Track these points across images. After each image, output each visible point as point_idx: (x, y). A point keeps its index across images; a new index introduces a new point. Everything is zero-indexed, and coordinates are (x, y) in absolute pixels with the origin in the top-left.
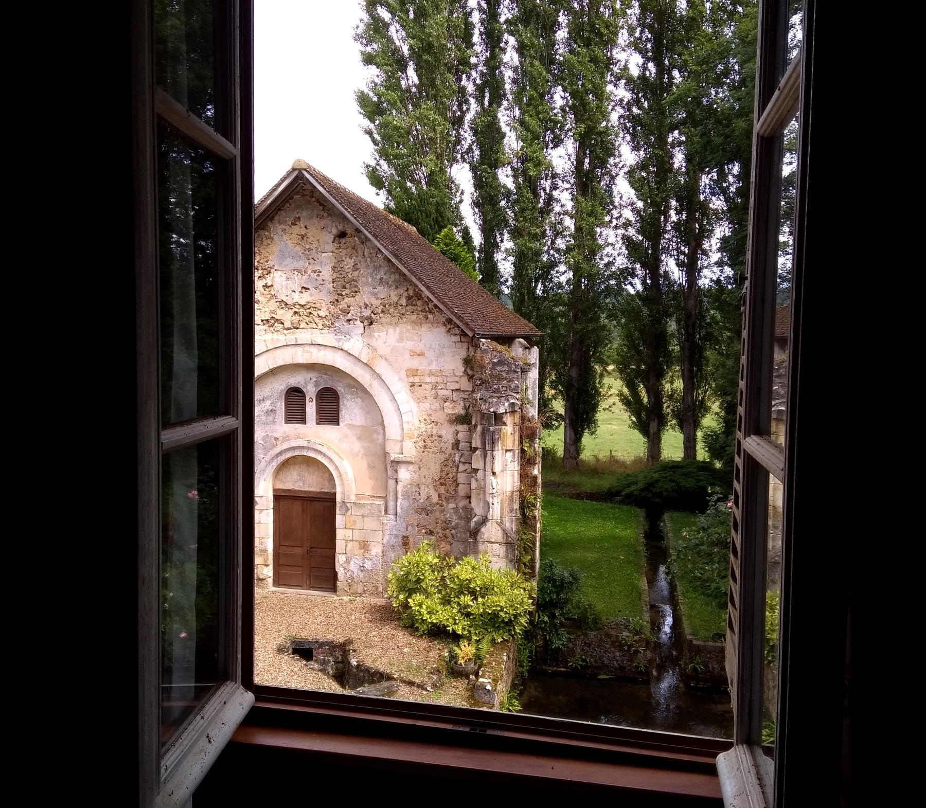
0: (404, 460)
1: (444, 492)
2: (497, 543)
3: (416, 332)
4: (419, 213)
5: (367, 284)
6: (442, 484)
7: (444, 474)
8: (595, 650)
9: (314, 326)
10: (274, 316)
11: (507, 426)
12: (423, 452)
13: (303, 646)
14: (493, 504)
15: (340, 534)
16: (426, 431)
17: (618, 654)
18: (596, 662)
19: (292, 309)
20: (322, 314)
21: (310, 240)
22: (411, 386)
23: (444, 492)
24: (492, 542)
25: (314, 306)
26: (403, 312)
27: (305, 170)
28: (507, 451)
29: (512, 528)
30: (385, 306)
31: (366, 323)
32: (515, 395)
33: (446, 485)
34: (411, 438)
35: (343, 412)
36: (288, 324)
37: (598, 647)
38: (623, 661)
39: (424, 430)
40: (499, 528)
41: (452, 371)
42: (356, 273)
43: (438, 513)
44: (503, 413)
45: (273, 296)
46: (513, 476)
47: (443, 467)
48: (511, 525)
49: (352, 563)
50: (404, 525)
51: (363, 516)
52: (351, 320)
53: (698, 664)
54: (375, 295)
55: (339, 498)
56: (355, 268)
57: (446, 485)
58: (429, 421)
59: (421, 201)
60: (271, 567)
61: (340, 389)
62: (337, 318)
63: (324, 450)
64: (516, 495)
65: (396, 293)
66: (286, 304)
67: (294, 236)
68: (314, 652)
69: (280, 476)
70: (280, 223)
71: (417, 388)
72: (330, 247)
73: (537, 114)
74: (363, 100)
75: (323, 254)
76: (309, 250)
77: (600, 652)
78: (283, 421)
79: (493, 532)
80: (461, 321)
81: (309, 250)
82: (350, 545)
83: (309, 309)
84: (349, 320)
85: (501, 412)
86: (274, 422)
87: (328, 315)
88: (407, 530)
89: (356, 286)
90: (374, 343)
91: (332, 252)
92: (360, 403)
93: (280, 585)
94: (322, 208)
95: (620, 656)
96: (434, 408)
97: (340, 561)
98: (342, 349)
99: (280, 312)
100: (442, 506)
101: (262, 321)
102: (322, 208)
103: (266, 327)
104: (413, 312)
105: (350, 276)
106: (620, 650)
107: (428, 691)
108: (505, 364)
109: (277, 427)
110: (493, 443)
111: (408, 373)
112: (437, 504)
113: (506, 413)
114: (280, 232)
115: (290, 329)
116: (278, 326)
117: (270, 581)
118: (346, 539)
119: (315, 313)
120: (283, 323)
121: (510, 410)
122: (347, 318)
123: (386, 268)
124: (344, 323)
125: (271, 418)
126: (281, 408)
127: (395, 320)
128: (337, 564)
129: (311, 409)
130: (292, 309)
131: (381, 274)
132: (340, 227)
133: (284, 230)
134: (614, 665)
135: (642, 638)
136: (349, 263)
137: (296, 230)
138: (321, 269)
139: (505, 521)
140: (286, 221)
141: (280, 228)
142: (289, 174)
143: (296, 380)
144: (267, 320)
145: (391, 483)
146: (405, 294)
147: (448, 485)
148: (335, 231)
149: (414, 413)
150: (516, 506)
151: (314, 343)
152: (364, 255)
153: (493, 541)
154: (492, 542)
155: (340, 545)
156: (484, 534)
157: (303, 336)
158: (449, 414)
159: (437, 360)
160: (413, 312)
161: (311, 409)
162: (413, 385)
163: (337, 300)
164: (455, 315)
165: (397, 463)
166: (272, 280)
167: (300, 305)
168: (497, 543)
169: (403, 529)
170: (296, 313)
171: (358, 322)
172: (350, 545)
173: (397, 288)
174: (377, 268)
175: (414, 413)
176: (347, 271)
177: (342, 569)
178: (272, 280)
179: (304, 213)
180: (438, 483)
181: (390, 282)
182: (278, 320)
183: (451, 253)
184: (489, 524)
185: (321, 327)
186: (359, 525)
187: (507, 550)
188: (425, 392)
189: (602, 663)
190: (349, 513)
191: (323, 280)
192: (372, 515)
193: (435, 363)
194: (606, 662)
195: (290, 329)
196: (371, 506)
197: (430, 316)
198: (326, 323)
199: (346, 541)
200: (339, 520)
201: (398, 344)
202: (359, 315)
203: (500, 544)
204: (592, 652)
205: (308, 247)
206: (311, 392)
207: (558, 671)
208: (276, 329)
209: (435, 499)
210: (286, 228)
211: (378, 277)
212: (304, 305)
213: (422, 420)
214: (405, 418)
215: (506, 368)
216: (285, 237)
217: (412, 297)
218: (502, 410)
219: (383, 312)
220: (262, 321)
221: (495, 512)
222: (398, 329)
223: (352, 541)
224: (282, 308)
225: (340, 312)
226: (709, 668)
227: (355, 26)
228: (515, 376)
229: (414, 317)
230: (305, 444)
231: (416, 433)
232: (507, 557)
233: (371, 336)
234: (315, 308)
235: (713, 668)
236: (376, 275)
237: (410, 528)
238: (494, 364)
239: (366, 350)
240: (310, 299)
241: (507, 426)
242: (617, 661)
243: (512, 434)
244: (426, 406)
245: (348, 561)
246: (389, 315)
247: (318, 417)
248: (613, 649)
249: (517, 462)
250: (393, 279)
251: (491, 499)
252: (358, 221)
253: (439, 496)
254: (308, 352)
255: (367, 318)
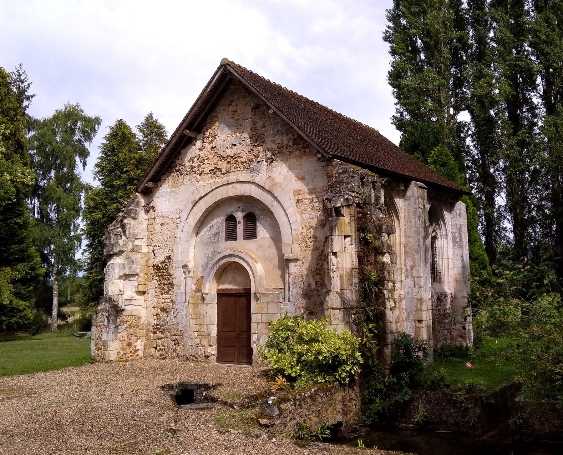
0: (292, 257)
1: (319, 280)
2: (338, 309)
3: (298, 163)
4: (420, 139)
5: (270, 135)
6: (318, 274)
7: (319, 266)
8: (434, 407)
9: (239, 169)
10: (216, 166)
11: (344, 217)
12: (305, 250)
13: (187, 388)
14: (333, 278)
15: (254, 317)
16: (307, 235)
17: (453, 411)
18: (436, 418)
19: (226, 160)
20: (243, 160)
21: (238, 114)
22: (297, 203)
23: (319, 280)
24: (334, 309)
25: (239, 156)
26: (291, 150)
27: (228, 64)
28: (345, 237)
29: (352, 298)
30: (280, 149)
31: (269, 162)
32: (351, 193)
33: (320, 274)
34: (297, 241)
35: (259, 229)
36: (224, 171)
37: (437, 404)
38: (457, 418)
39: (305, 234)
40: (338, 297)
41: (322, 188)
42: (264, 129)
43: (315, 297)
44: (340, 207)
45: (216, 153)
46: (351, 256)
47: (319, 261)
48: (351, 296)
49: (261, 340)
50: (294, 309)
51: (268, 303)
52: (260, 161)
53: (519, 419)
54: (274, 142)
55: (253, 291)
56: (264, 126)
57: (320, 274)
58: (308, 227)
59: (421, 131)
60: (215, 347)
61: (257, 212)
62: (252, 161)
63: (243, 256)
64: (355, 272)
65: (286, 138)
66: (223, 158)
67: (230, 112)
68: (194, 392)
69: (221, 280)
70: (222, 106)
71: (300, 204)
72: (249, 116)
73: (505, 62)
74: (389, 73)
75: (246, 121)
76: (238, 119)
77: (439, 409)
78: (224, 240)
79: (335, 300)
80: (320, 147)
81: (238, 119)
82: (260, 325)
83: (236, 158)
84: (259, 162)
85: (338, 205)
86: (218, 241)
87: (247, 160)
88: (296, 312)
89: (263, 138)
90: (273, 176)
91: (251, 118)
92: (269, 221)
93: (221, 361)
94: (245, 91)
95: (455, 413)
96: (311, 216)
97: (254, 339)
98: (254, 183)
99: (220, 163)
100: (318, 291)
101: (210, 171)
102: (245, 91)
103: (212, 175)
104: (297, 150)
105: (260, 132)
106: (454, 408)
107: (235, 408)
108: (347, 172)
109: (220, 244)
110: (332, 229)
111: (295, 194)
112: (315, 289)
113: (343, 207)
114: (222, 111)
115: (225, 173)
116: (219, 173)
117: (214, 358)
118: (257, 321)
119: (239, 161)
120: (221, 171)
121: (346, 204)
122: (258, 160)
123: (282, 123)
124: (256, 164)
125: (217, 238)
126: (223, 231)
127: (286, 156)
128: (252, 342)
129: (240, 229)
130: (226, 160)
131: (279, 127)
132: (256, 101)
133: (224, 110)
134: (450, 420)
135: (472, 396)
136: (260, 123)
137: (231, 108)
138: (244, 131)
139: (347, 292)
140: (225, 104)
141: (222, 108)
142: (219, 69)
143: (229, 210)
144: (212, 170)
145: (287, 275)
146: (292, 138)
147: (322, 275)
148: (252, 104)
149: (299, 222)
150: (356, 280)
151: (238, 181)
152: (269, 117)
153: (335, 307)
154: (334, 309)
155: (254, 326)
156: (328, 302)
157: (232, 177)
158: (321, 220)
159: (312, 181)
160: (297, 150)
161: (240, 229)
162: (298, 201)
163: (252, 150)
164: (316, 144)
165: (289, 261)
166: (216, 143)
167: (231, 156)
168: (338, 309)
169: (293, 311)
170: (229, 162)
171: (264, 162)
172: (260, 325)
173: (287, 134)
174: (276, 124)
175: (299, 222)
176: (259, 129)
177: (255, 345)
178: (216, 143)
179: (236, 96)
180: (315, 273)
181: (283, 132)
182: (219, 169)
183: (440, 161)
184: (331, 293)
185: (242, 169)
186: (265, 310)
187: (344, 314)
188: (306, 206)
189: (441, 419)
190: (259, 302)
191: (244, 138)
192: (273, 302)
193: (311, 183)
194: (444, 418)
195: (225, 173)
196: (273, 295)
197: (307, 150)
198: (246, 166)
199: (258, 323)
200: (254, 306)
201: (287, 174)
202: (265, 157)
203: (339, 309)
204: (433, 410)
205: (237, 118)
206: (239, 216)
207: (407, 427)
208: (218, 175)
209: (314, 286)
210: (226, 108)
211: (277, 129)
212: (233, 156)
213: (304, 226)
214: (293, 227)
215: (347, 175)
216: (225, 114)
217: (297, 139)
218: (339, 205)
219: (279, 153)
220: (210, 171)
221: (335, 283)
222: (288, 163)
223: (261, 323)
224: (221, 161)
225: (253, 157)
226: (530, 423)
227: (385, 31)
228: (352, 180)
229: (297, 153)
230: (232, 253)
231: (300, 237)
232: (344, 319)
233: (272, 171)
234: (240, 157)
235: (534, 424)
236: (275, 128)
237: (298, 310)
238: (340, 174)
239: (268, 181)
240: (236, 151)
241: (344, 217)
242: (453, 417)
243: (349, 223)
244: (306, 216)
245: (258, 340)
246: (282, 154)
247: (245, 234)
248: (448, 407)
249: (354, 245)
250: (285, 129)
251: (332, 273)
252: (257, 90)
253: (316, 283)
254: (235, 187)
255: (269, 158)
